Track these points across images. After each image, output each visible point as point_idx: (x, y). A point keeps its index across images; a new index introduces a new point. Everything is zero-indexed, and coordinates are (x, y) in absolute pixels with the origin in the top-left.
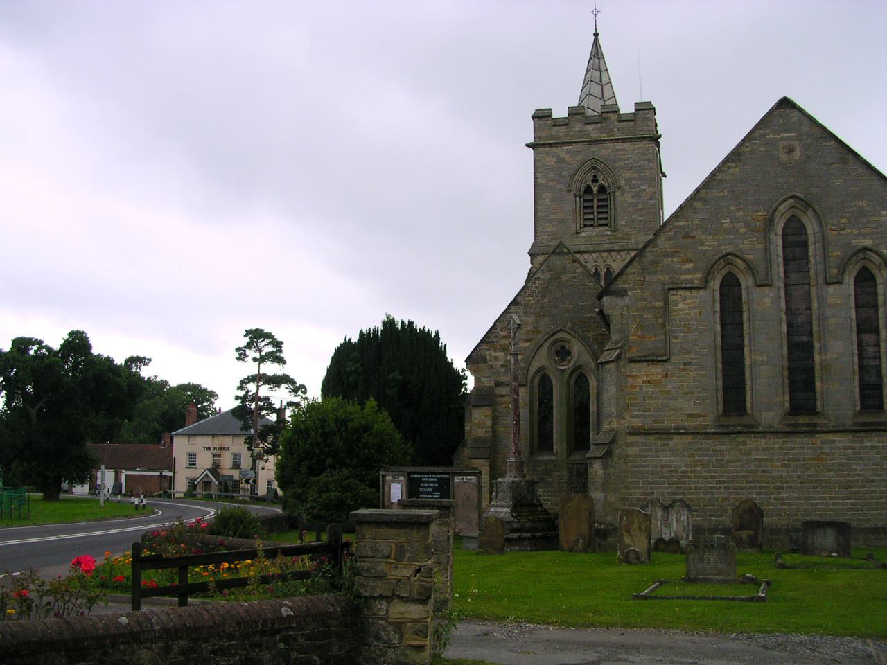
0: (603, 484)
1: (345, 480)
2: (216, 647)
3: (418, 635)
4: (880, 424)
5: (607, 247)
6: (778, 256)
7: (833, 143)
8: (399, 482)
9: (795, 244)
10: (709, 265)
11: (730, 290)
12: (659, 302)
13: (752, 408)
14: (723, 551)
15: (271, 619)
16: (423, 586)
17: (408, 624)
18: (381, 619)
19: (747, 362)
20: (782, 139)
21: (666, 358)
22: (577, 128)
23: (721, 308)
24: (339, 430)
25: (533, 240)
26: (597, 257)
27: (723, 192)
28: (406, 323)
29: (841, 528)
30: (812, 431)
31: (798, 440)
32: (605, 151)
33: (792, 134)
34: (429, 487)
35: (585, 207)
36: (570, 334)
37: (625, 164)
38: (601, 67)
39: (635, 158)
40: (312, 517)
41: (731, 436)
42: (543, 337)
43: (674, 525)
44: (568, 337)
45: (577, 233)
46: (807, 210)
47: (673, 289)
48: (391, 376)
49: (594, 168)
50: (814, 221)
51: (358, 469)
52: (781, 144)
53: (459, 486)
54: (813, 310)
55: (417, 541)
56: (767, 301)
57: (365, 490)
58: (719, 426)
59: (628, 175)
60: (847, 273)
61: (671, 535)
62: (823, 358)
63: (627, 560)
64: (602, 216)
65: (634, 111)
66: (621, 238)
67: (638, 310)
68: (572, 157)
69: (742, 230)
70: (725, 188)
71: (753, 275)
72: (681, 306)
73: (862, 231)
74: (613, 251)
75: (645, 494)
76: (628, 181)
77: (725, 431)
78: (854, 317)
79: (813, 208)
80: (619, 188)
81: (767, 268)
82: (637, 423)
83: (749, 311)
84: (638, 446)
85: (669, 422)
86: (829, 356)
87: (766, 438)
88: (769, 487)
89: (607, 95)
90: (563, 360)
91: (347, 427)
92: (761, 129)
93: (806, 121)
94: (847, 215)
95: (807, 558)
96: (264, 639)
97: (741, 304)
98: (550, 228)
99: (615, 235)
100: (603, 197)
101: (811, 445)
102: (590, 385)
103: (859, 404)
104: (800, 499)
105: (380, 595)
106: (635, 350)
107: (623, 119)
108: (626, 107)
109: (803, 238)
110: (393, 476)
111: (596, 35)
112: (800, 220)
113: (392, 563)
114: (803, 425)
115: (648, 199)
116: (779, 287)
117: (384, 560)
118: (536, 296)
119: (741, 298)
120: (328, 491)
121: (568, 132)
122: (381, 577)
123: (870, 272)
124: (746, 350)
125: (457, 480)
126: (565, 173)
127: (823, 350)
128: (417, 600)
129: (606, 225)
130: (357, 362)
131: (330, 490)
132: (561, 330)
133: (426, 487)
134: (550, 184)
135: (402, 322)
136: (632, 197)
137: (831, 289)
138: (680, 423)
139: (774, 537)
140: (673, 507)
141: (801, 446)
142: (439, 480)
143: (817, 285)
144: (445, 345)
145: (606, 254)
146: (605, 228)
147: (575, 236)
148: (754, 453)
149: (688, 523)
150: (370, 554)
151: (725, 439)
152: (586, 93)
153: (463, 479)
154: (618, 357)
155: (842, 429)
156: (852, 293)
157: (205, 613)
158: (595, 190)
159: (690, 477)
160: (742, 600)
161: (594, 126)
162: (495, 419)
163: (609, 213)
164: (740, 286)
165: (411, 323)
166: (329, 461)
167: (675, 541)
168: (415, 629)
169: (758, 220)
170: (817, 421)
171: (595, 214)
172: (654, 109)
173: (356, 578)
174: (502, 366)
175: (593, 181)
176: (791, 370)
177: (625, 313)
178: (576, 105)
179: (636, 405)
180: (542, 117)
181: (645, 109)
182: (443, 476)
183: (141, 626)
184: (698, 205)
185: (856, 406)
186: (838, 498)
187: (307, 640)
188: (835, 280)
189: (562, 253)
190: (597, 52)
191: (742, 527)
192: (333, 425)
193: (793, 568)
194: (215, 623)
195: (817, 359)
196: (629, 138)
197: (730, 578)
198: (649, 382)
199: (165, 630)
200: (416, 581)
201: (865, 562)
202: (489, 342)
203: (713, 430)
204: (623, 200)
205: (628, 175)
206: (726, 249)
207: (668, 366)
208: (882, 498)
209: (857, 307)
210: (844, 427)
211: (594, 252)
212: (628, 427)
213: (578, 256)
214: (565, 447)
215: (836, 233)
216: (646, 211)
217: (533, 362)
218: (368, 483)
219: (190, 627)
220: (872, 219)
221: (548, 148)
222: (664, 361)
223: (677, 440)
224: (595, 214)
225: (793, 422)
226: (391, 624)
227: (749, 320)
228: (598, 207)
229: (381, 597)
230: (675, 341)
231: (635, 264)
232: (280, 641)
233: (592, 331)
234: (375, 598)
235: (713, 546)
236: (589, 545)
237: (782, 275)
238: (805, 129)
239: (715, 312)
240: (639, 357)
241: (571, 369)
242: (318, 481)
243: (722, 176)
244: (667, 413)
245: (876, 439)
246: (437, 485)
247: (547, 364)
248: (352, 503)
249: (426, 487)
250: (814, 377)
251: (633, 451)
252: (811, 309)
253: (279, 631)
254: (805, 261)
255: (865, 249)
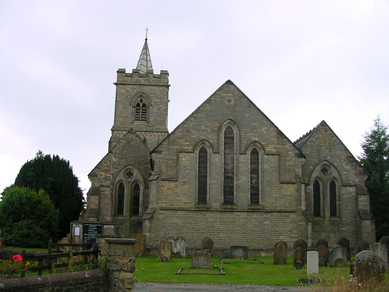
0: (149, 230)
1: (29, 225)
2: (67, 289)
3: (130, 284)
4: (258, 209)
5: (145, 129)
6: (222, 142)
7: (246, 99)
8: (79, 227)
9: (229, 139)
10: (196, 144)
11: (203, 152)
12: (175, 157)
13: (209, 201)
14: (206, 257)
15: (83, 278)
16: (132, 266)
17: (126, 280)
18: (116, 278)
19: (208, 183)
20: (227, 96)
21: (176, 180)
22: (136, 78)
23: (199, 161)
24: (27, 203)
25: (114, 124)
26: (140, 134)
27: (203, 115)
28: (55, 156)
29: (245, 249)
30: (232, 211)
31: (226, 214)
32: (146, 89)
33: (231, 95)
34: (93, 229)
35: (136, 112)
36: (133, 166)
37: (154, 96)
38: (147, 53)
39: (159, 93)
40: (15, 241)
41: (201, 212)
42: (122, 167)
43: (178, 247)
44: (132, 168)
45: (132, 123)
46: (235, 125)
47: (181, 152)
48: (49, 179)
49: (141, 96)
50: (237, 129)
51: (36, 220)
52: (226, 98)
53: (106, 229)
54: (234, 164)
55: (131, 250)
56: (217, 159)
57: (38, 229)
58: (196, 208)
59: (156, 100)
60: (248, 150)
61: (177, 251)
62: (238, 183)
63: (162, 260)
64: (143, 116)
65: (160, 74)
66: (151, 126)
67: (166, 159)
68: (132, 90)
69: (209, 131)
70: (203, 113)
71: (212, 148)
72: (183, 159)
73: (255, 134)
74: (147, 132)
75: (165, 234)
76: (155, 103)
77: (198, 210)
78: (250, 167)
79: (237, 124)
80: (151, 105)
81: (218, 146)
82: (164, 205)
83: (210, 162)
84: (163, 215)
85: (176, 206)
86: (240, 182)
87: (214, 213)
88: (215, 233)
89: (149, 65)
90: (129, 177)
91: (31, 201)
92: (219, 91)
93: (236, 90)
94: (249, 128)
95: (233, 260)
96: (81, 286)
97: (207, 160)
98: (121, 120)
99: (148, 125)
100: (144, 108)
101: (231, 216)
102: (140, 188)
103: (250, 201)
104: (226, 237)
105: (117, 269)
106: (164, 176)
107: (155, 77)
108: (157, 72)
109: (232, 135)
110: (76, 225)
111: (146, 40)
112: (231, 128)
113: (121, 258)
114: (229, 209)
115: (163, 111)
116: (222, 154)
117: (119, 257)
118: (120, 150)
119: (207, 158)
120: (22, 229)
121: (132, 80)
122: (117, 263)
123: (257, 150)
124: (208, 178)
125: (105, 227)
126: (129, 97)
127: (238, 179)
128: (130, 271)
129: (145, 120)
130: (33, 172)
131: (24, 229)
132: (129, 165)
133: (91, 229)
134: (122, 101)
135: (54, 156)
136: (156, 110)
137: (242, 156)
138: (181, 206)
139: (216, 252)
140: (178, 240)
141: (228, 217)
142: (97, 227)
143: (237, 154)
144: (72, 167)
145: (144, 132)
146: (144, 122)
147: (131, 124)
148: (209, 219)
149: (184, 246)
150: (113, 254)
151: (198, 213)
152: (140, 64)
153: (108, 227)
154: (157, 178)
155: (243, 210)
156: (250, 158)
157: (63, 276)
158: (141, 105)
159: (184, 228)
160: (217, 275)
161: (143, 78)
162: (100, 201)
163: (146, 115)
164: (207, 153)
165: (57, 156)
166: (23, 216)
167: (178, 253)
168: (129, 282)
169: (215, 127)
170: (234, 207)
171: (141, 115)
172: (168, 74)
173: (108, 263)
174: (104, 178)
175: (140, 101)
176: (225, 187)
177: (161, 160)
178: (135, 69)
179: (163, 198)
180: (121, 72)
181: (165, 74)
182: (99, 225)
183: (45, 281)
184: (192, 119)
185: (249, 202)
186: (241, 237)
187: (93, 286)
188: (244, 153)
189: (132, 133)
190: (146, 47)
191: (205, 248)
192: (25, 200)
193: (229, 264)
194: (67, 280)
195: (235, 183)
196: (157, 85)
197: (209, 267)
198: (169, 189)
199: (53, 282)
200: (130, 264)
201: (254, 261)
202: (99, 168)
203: (194, 209)
204: (153, 111)
205: (156, 100)
206: (203, 137)
207: (177, 183)
208: (257, 237)
209: (251, 164)
210: (244, 210)
211: (139, 131)
212: (160, 207)
213: (136, 132)
214: (129, 214)
215: (245, 134)
216: (161, 116)
217: (117, 177)
218: (39, 226)
219: (60, 281)
220: (259, 130)
221: (122, 86)
222: (175, 181)
223: (179, 213)
224: (141, 115)
225: (225, 207)
226: (120, 280)
227: (210, 166)
228: (142, 112)
229: (117, 270)
230: (180, 173)
231: (166, 141)
232: (85, 287)
233: (143, 166)
234: (114, 271)
235: (202, 255)
236: (144, 254)
237: (223, 149)
238: (236, 93)
239: (196, 162)
240: (165, 178)
241: (133, 181)
242: (18, 225)
243: (203, 109)
244: (176, 202)
245: (256, 215)
246: (96, 229)
247: (123, 179)
248: (33, 235)
249: (91, 229)
250: (233, 190)
251: (161, 216)
252: (234, 163)
253: (85, 283)
254: (232, 145)
255: (256, 141)
